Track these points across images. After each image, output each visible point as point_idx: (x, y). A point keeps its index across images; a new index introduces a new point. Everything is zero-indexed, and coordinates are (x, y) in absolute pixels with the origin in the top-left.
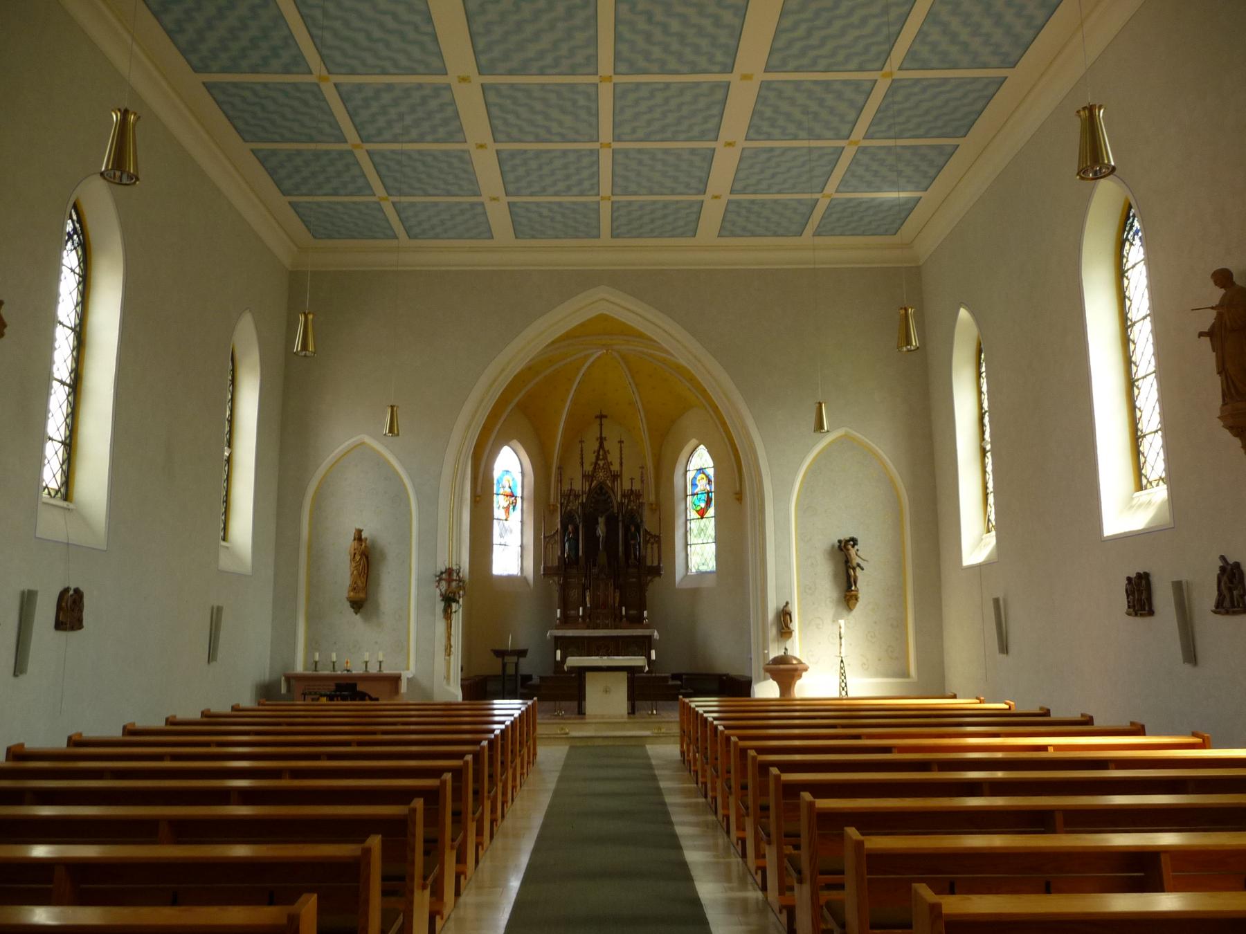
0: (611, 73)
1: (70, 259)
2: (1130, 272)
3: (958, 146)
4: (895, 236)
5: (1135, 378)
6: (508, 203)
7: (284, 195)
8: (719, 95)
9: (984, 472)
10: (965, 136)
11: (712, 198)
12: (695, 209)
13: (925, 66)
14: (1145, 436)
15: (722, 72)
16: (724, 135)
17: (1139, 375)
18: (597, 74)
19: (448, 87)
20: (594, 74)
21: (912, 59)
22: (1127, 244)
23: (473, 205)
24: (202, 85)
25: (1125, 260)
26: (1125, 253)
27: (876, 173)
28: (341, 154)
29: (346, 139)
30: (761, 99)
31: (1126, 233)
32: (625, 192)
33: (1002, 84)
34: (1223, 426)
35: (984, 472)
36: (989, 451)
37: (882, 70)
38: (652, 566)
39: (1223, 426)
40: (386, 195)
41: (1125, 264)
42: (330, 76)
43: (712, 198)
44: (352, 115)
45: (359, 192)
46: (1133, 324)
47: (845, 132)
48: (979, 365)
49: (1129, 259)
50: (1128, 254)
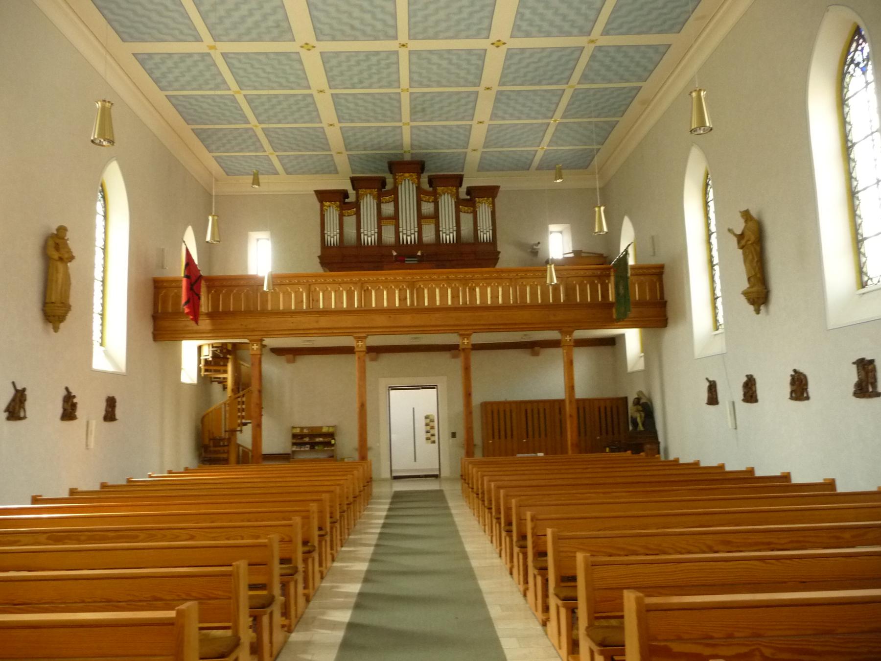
0: (408, 87)
1: (99, 206)
2: (849, 101)
3: (641, 87)
4: (679, 34)
5: (856, 190)
6: (332, 94)
7: (161, 90)
8: (472, 97)
9: (713, 281)
10: (679, 32)
11: (478, 123)
12: (472, 97)
13: (593, 82)
14: (865, 239)
15: (463, 148)
16: (477, 117)
17: (859, 188)
18: (399, 88)
19: (311, 95)
20: (401, 128)
21: (584, 78)
22: (848, 76)
23: (305, 96)
24: (165, 97)
25: (845, 90)
26: (845, 85)
27: (613, 60)
28: (246, 130)
29: (202, 40)
30: (497, 100)
31: (846, 67)
32: (421, 85)
33: (640, 89)
34: (745, 293)
35: (713, 281)
36: (717, 264)
37: (567, 84)
38: (494, 283)
39: (745, 293)
40: (239, 89)
41: (846, 94)
42: (241, 91)
43: (478, 123)
44: (204, 17)
45: (217, 87)
46: (854, 144)
47: (550, 115)
48: (706, 193)
49: (849, 89)
50: (848, 85)
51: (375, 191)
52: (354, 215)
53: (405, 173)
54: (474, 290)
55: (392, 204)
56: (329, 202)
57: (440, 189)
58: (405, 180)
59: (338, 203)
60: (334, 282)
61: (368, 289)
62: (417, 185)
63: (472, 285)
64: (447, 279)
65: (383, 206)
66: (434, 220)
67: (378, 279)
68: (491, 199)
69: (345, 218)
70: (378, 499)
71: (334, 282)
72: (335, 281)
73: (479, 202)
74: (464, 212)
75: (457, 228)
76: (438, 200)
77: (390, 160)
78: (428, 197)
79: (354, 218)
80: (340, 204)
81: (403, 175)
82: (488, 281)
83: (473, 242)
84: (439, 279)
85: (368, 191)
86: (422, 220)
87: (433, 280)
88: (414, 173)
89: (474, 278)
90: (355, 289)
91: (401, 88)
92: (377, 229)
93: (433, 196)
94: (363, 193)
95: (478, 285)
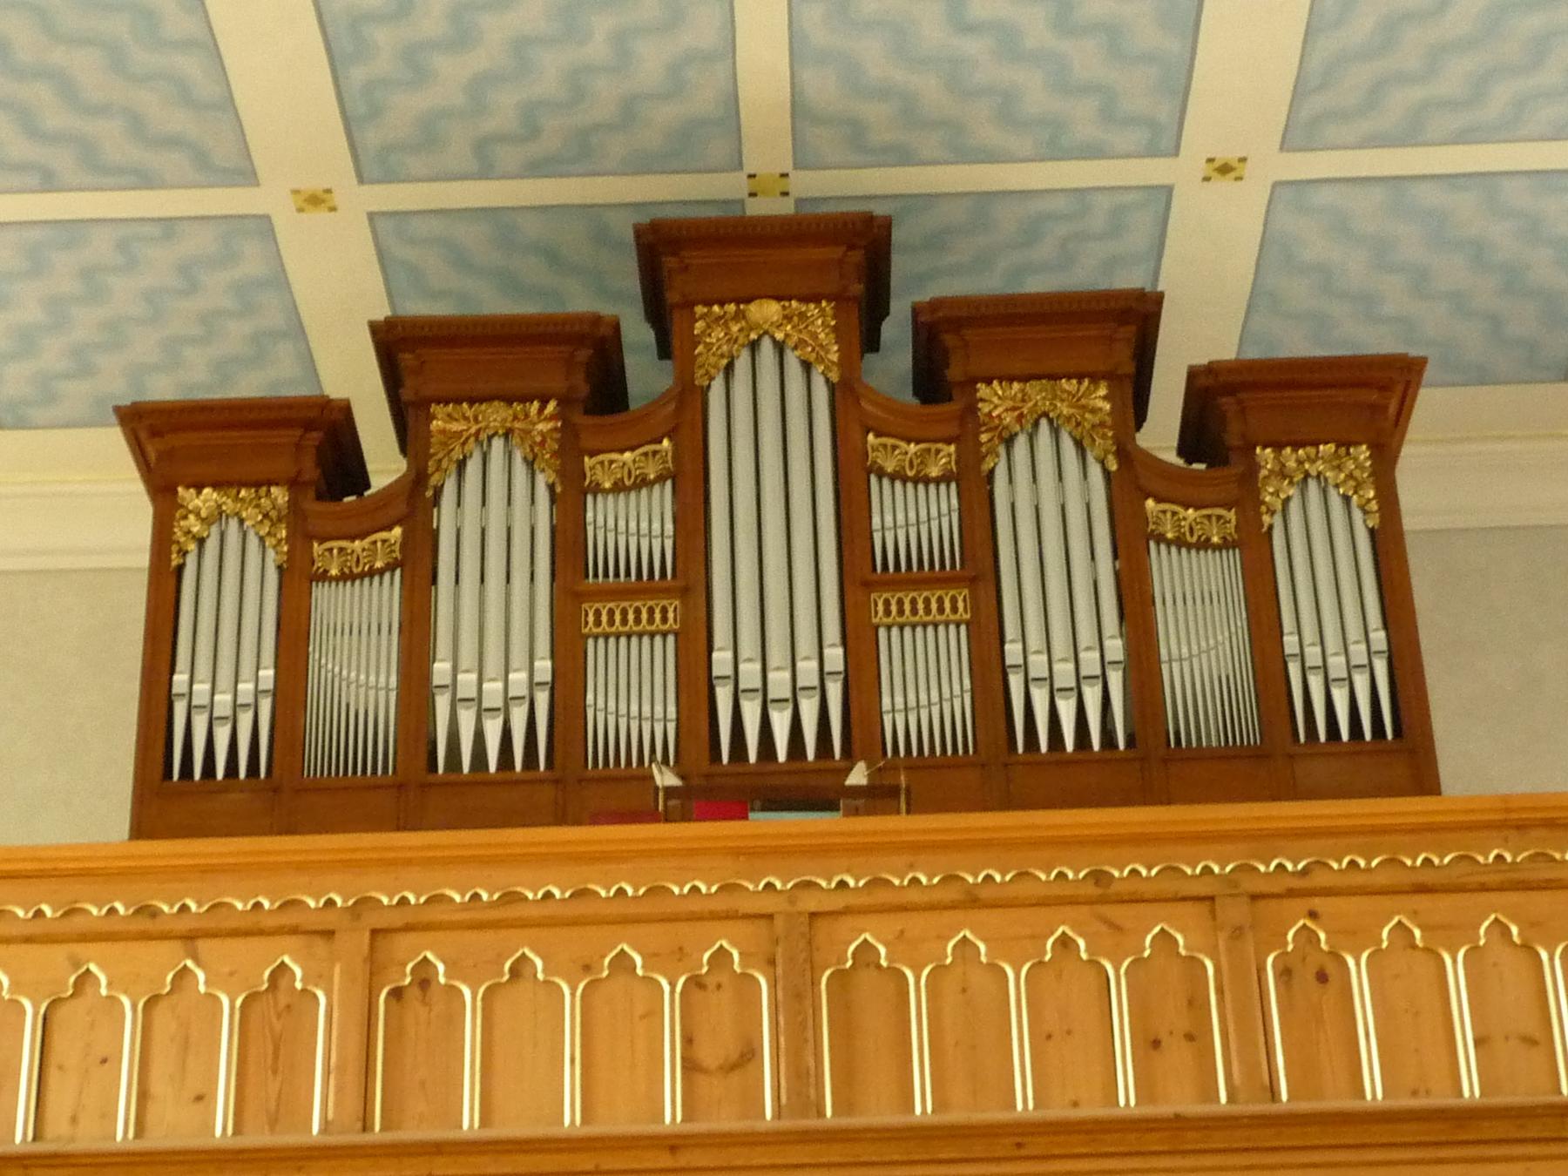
0: (787, 167)
19: (264, 226)
51: (543, 421)
52: (390, 567)
53: (749, 301)
54: (1328, 976)
55: (661, 500)
56: (216, 486)
57: (995, 399)
58: (754, 346)
59: (280, 495)
60: (145, 924)
61: (424, 978)
62: (834, 376)
63: (1307, 935)
64: (1091, 890)
65: (601, 514)
66: (962, 595)
67: (511, 898)
68: (1363, 452)
69: (322, 594)
70: (1530, 856)
71: (145, 924)
72: (155, 913)
73: (1282, 473)
74: (1180, 543)
75: (1128, 649)
76: (987, 465)
77: (645, 219)
78: (913, 448)
79: (386, 596)
80: (293, 504)
81: (739, 316)
82: (1442, 907)
83: (1254, 738)
84: (1025, 889)
85: (496, 414)
86: (879, 599)
87: (973, 901)
88: (815, 299)
89: (1319, 879)
90: (317, 976)
91: (748, 169)
92: (553, 656)
93: (948, 442)
94: (455, 427)
95: (1358, 936)
